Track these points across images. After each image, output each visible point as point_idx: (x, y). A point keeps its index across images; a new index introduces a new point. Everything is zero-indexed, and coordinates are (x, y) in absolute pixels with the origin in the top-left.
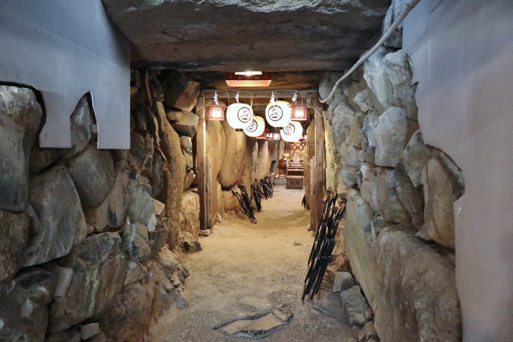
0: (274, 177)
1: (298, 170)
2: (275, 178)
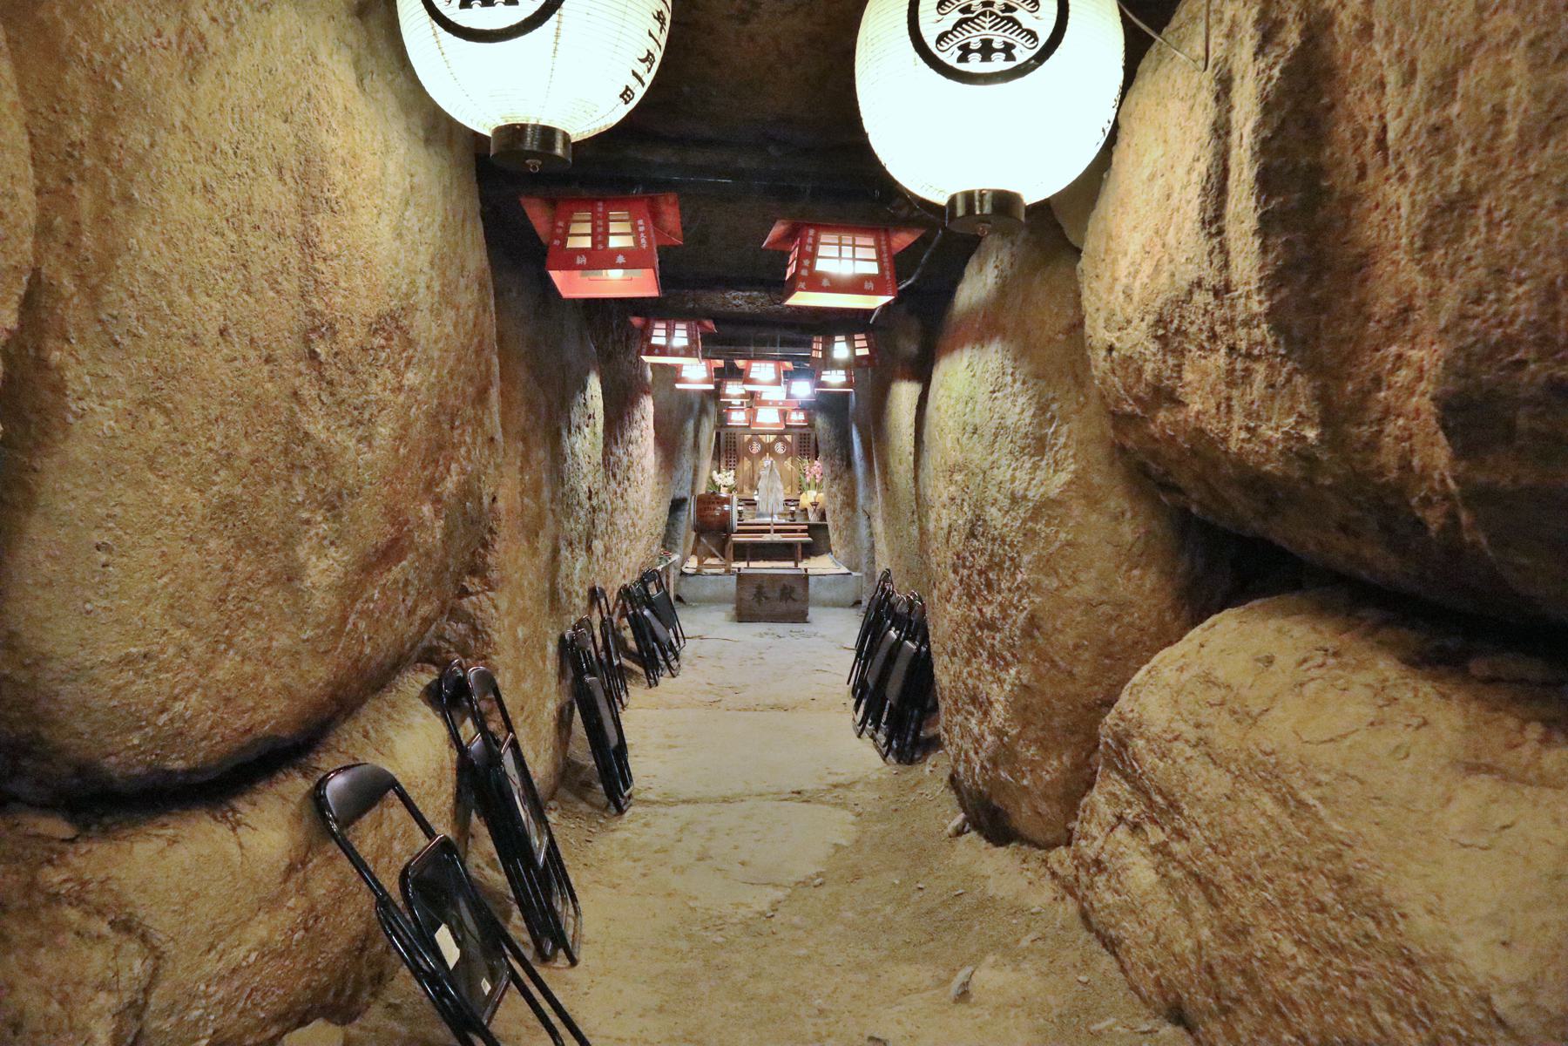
0: (678, 572)
1: (778, 538)
2: (683, 574)
